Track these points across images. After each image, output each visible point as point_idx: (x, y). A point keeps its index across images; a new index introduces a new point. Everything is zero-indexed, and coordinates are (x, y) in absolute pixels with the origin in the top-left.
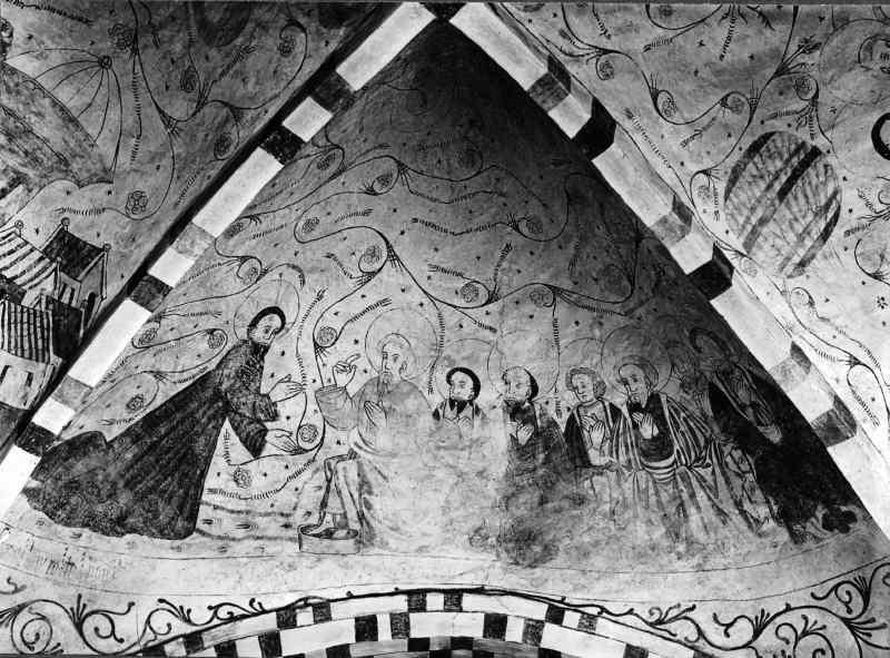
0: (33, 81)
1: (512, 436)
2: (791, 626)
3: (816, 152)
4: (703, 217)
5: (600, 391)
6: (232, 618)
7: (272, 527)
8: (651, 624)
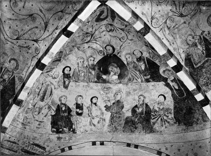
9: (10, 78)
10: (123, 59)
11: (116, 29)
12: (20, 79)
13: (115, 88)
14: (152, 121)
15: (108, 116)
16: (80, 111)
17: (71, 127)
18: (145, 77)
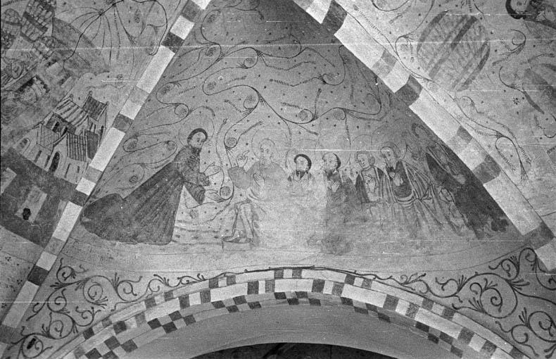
0: (69, 25)
1: (328, 188)
2: (479, 284)
3: (473, 19)
4: (404, 61)
5: (372, 162)
6: (188, 283)
7: (208, 238)
8: (401, 284)
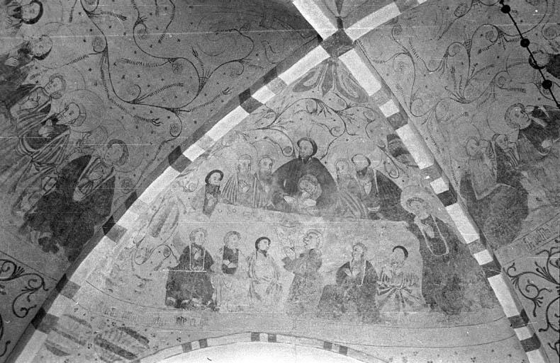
5: (55, 96)
9: (103, 180)
10: (331, 167)
11: (326, 111)
12: (126, 183)
13: (308, 224)
14: (377, 298)
15: (287, 279)
16: (232, 264)
17: (209, 297)
18: (369, 208)
